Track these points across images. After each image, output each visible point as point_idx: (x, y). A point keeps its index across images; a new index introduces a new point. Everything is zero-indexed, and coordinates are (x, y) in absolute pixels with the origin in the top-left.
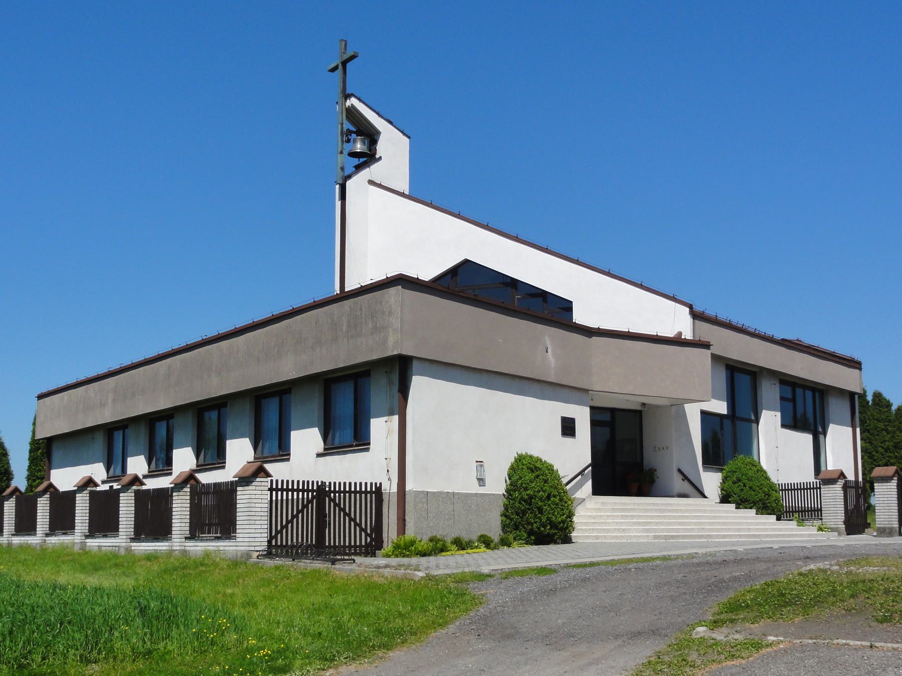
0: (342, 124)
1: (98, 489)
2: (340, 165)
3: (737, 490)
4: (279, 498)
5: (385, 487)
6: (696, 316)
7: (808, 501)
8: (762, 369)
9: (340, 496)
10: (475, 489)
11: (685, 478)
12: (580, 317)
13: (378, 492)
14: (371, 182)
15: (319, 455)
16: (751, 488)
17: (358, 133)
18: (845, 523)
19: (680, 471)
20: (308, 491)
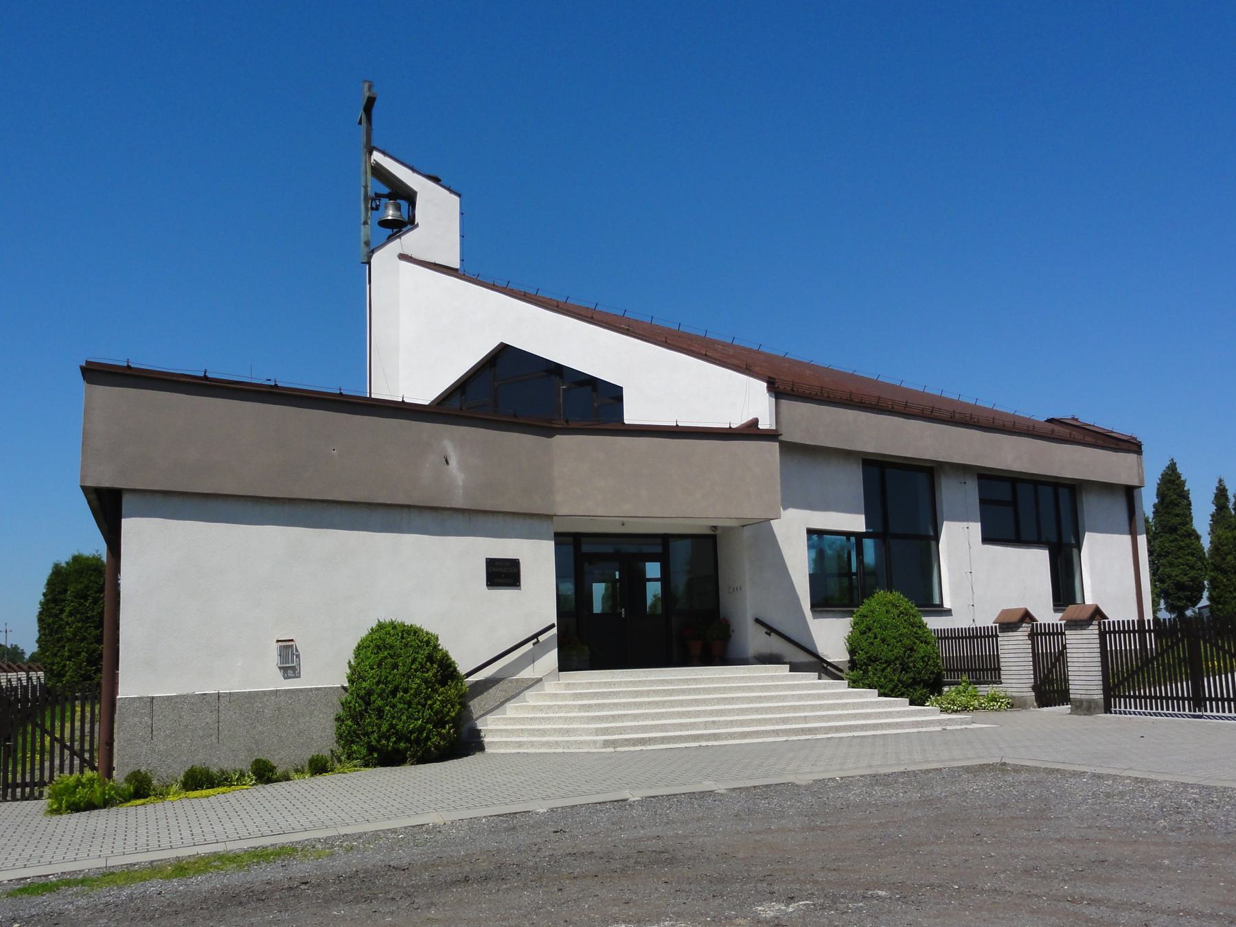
0: (366, 187)
2: (363, 239)
3: (865, 644)
6: (778, 390)
8: (941, 465)
10: (273, 681)
11: (771, 630)
14: (403, 257)
16: (883, 640)
17: (390, 196)
18: (1034, 688)
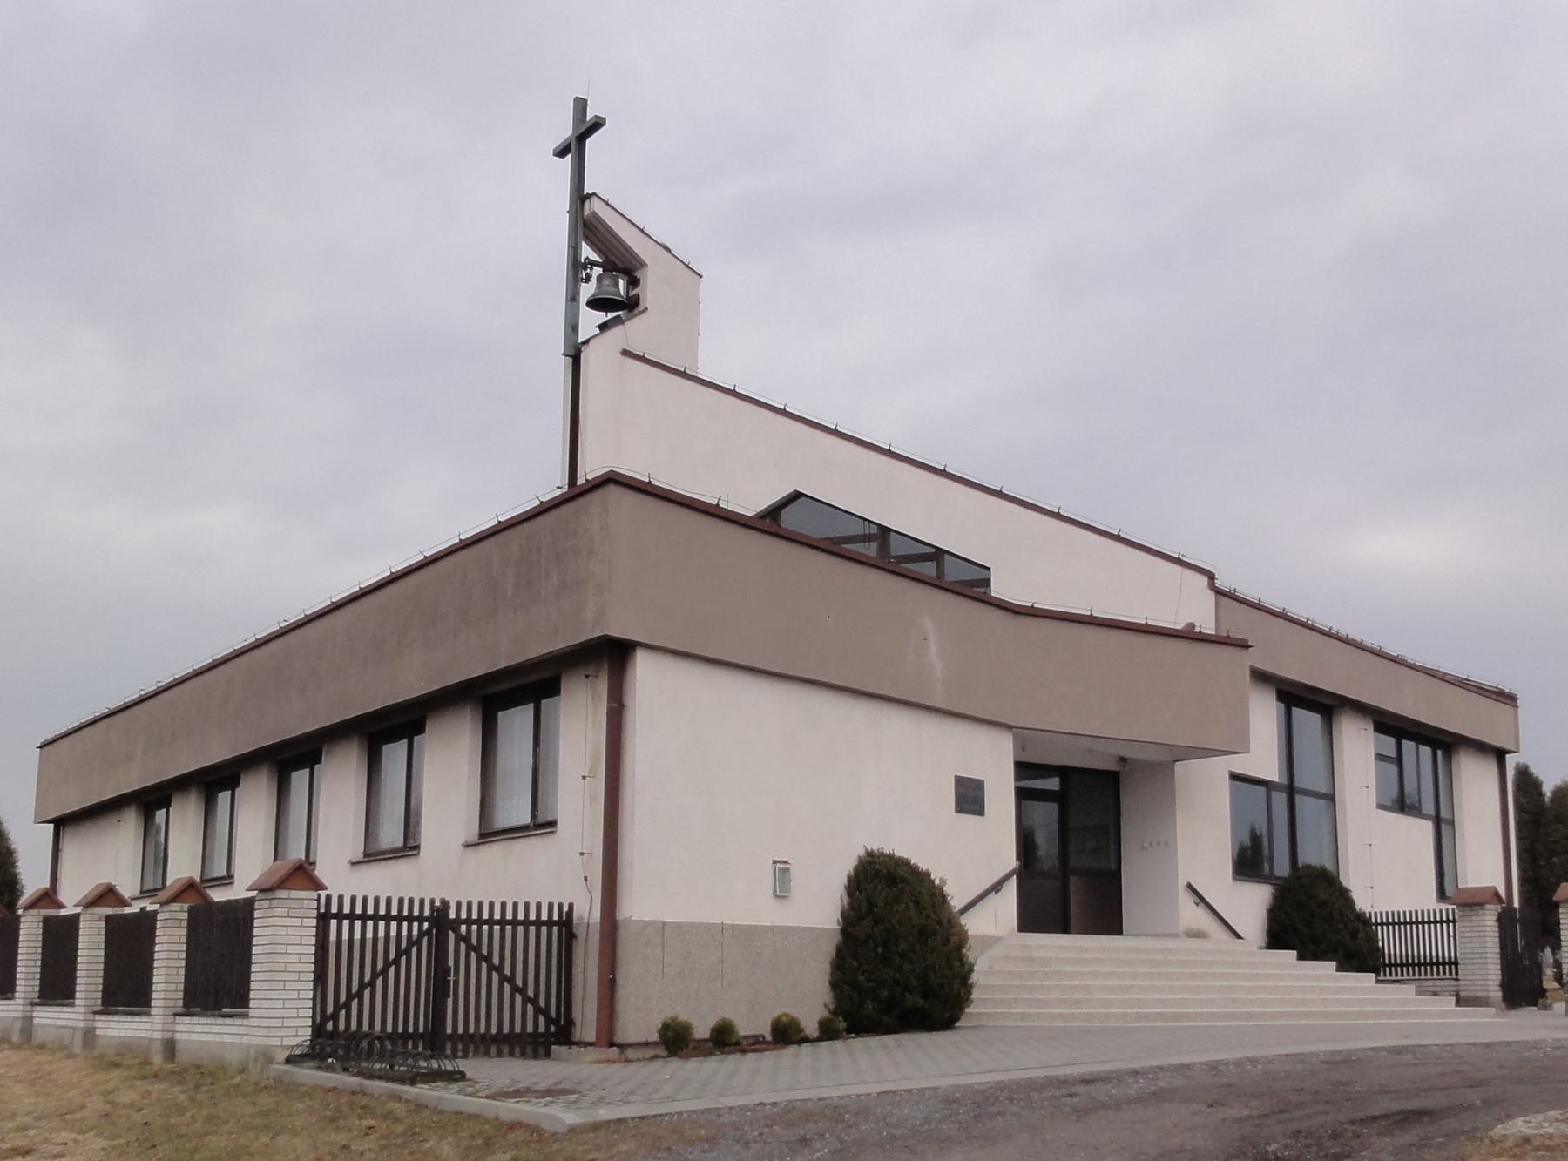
1: (127, 910)
4: (345, 936)
5: (580, 912)
7: (1432, 945)
9: (503, 931)
12: (998, 590)
13: (565, 925)
15: (467, 846)
19: (1190, 887)
20: (410, 919)
